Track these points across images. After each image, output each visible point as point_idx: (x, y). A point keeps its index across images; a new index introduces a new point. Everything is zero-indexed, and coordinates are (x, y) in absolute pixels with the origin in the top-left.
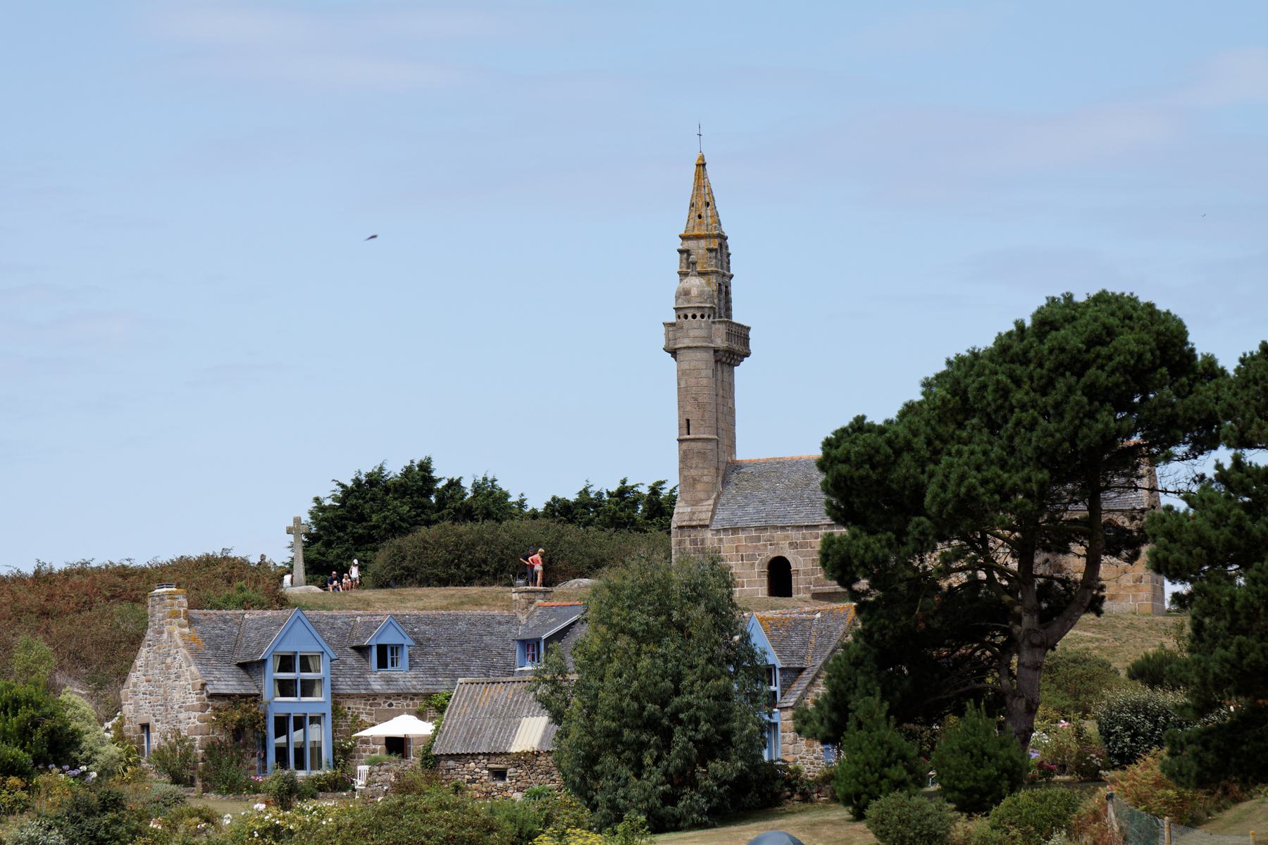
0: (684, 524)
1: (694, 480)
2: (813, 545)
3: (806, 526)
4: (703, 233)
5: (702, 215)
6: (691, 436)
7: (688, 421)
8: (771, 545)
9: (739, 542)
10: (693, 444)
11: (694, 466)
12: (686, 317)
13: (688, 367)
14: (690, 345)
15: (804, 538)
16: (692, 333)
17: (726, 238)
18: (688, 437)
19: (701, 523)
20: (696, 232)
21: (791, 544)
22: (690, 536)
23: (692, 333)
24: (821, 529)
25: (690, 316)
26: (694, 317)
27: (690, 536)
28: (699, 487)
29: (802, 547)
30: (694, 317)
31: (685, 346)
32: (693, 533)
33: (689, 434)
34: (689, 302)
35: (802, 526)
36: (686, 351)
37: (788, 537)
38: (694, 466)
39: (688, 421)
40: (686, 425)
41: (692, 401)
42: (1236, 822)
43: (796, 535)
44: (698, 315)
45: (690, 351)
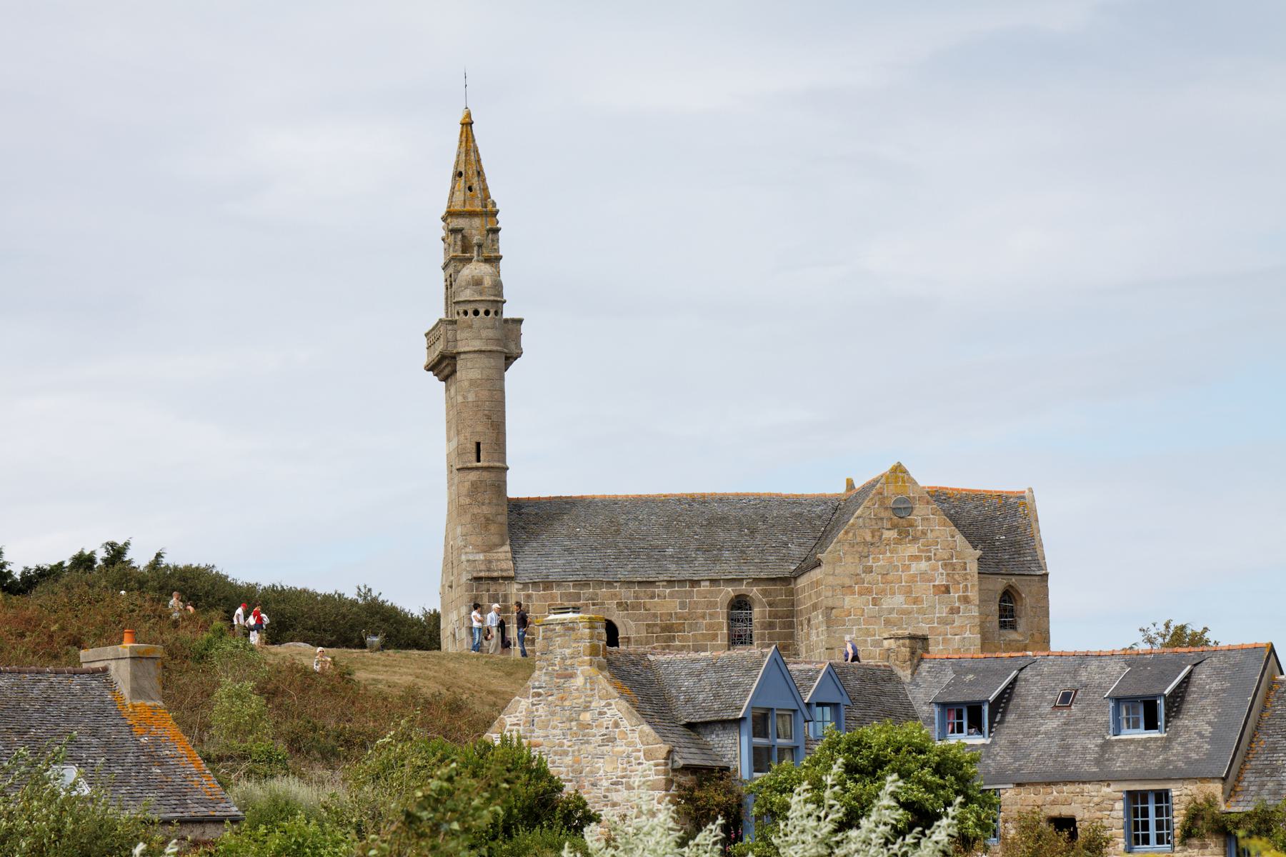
0: (482, 574)
2: (648, 607)
3: (639, 582)
7: (478, 444)
8: (594, 605)
9: (552, 599)
11: (487, 501)
12: (476, 313)
15: (637, 598)
19: (505, 574)
20: (468, 208)
21: (619, 604)
22: (488, 590)
24: (616, 587)
26: (487, 313)
27: (488, 590)
29: (633, 608)
31: (476, 349)
32: (493, 588)
33: (478, 460)
34: (481, 294)
35: (634, 582)
36: (476, 355)
37: (615, 595)
39: (478, 444)
40: (474, 450)
43: (627, 594)
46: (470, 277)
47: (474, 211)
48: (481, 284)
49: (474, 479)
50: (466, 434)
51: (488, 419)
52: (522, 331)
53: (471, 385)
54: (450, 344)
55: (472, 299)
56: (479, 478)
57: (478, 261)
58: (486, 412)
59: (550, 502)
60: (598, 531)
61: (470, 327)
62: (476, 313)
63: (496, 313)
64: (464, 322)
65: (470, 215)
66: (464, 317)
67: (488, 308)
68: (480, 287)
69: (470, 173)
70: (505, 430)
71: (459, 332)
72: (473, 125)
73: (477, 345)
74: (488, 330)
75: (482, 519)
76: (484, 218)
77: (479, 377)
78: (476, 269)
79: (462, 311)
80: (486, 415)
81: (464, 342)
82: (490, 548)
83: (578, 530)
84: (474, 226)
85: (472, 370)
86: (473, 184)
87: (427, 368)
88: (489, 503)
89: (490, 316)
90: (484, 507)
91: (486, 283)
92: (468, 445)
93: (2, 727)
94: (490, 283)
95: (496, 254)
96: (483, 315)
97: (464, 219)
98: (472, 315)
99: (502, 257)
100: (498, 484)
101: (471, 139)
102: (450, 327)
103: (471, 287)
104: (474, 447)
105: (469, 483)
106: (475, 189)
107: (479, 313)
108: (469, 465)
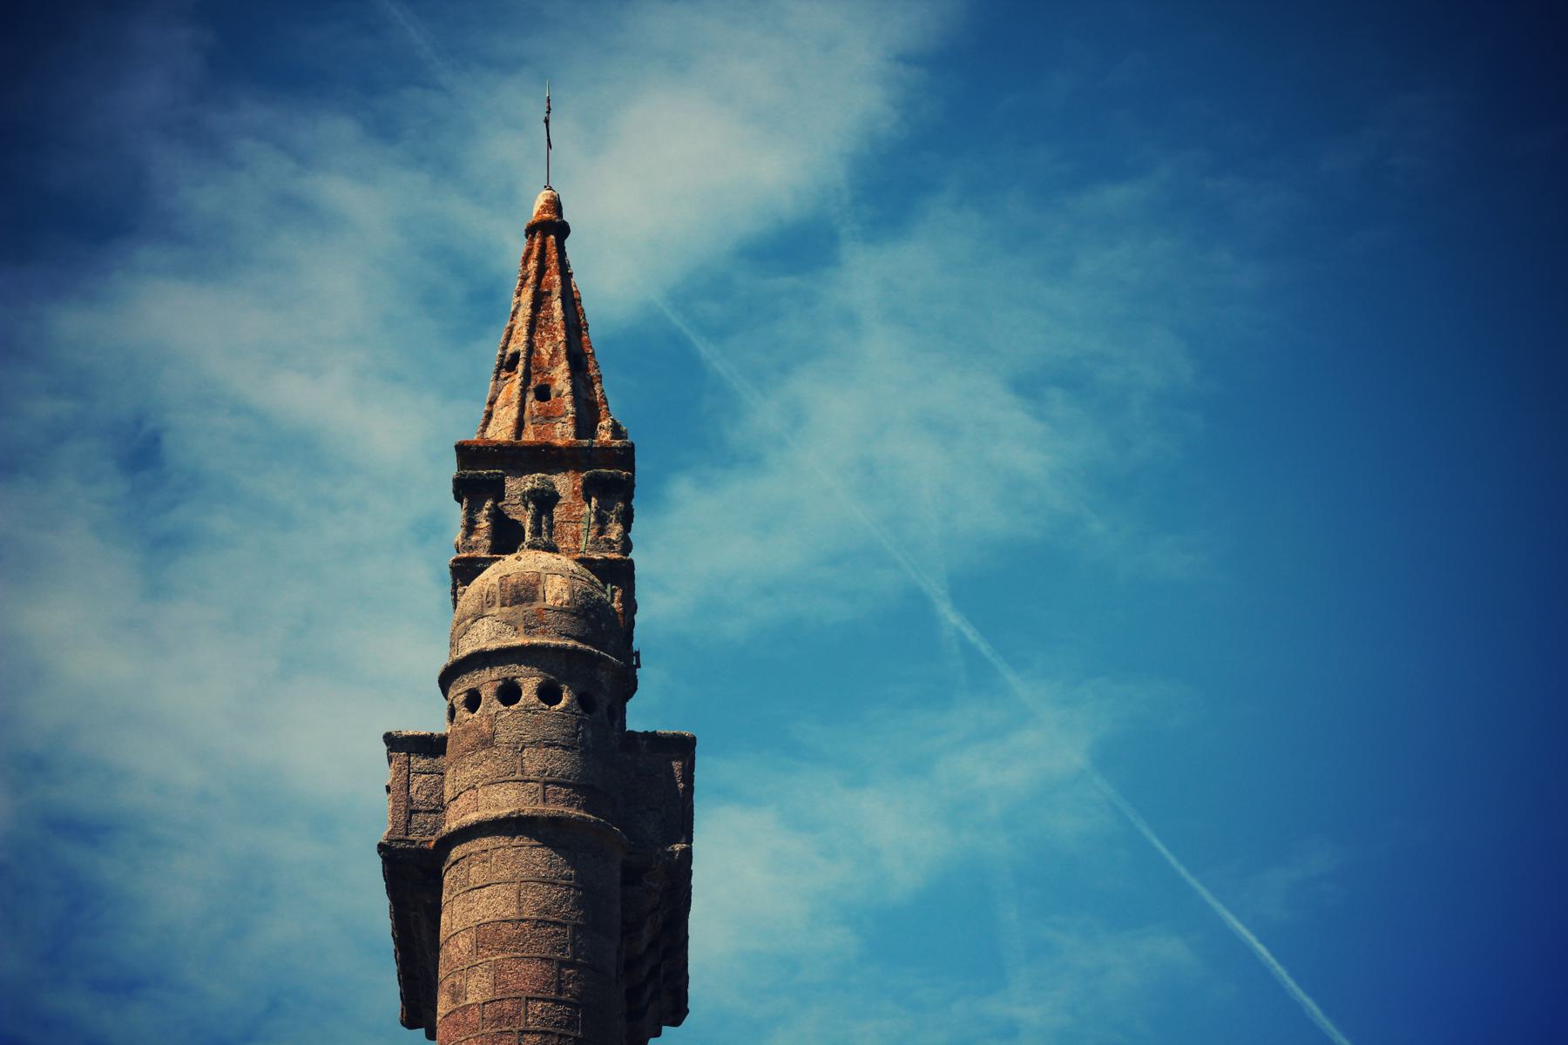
34: (529, 630)
48: (533, 599)
52: (642, 731)
53: (478, 945)
54: (418, 819)
61: (488, 742)
68: (525, 608)
69: (545, 352)
70: (688, 917)
71: (449, 774)
73: (505, 801)
77: (511, 912)
81: (461, 802)
82: (850, 320)
85: (486, 891)
86: (554, 380)
91: (549, 597)
98: (496, 703)
101: (553, 266)
102: (421, 763)
103: (496, 610)
106: (559, 395)
107: (520, 693)
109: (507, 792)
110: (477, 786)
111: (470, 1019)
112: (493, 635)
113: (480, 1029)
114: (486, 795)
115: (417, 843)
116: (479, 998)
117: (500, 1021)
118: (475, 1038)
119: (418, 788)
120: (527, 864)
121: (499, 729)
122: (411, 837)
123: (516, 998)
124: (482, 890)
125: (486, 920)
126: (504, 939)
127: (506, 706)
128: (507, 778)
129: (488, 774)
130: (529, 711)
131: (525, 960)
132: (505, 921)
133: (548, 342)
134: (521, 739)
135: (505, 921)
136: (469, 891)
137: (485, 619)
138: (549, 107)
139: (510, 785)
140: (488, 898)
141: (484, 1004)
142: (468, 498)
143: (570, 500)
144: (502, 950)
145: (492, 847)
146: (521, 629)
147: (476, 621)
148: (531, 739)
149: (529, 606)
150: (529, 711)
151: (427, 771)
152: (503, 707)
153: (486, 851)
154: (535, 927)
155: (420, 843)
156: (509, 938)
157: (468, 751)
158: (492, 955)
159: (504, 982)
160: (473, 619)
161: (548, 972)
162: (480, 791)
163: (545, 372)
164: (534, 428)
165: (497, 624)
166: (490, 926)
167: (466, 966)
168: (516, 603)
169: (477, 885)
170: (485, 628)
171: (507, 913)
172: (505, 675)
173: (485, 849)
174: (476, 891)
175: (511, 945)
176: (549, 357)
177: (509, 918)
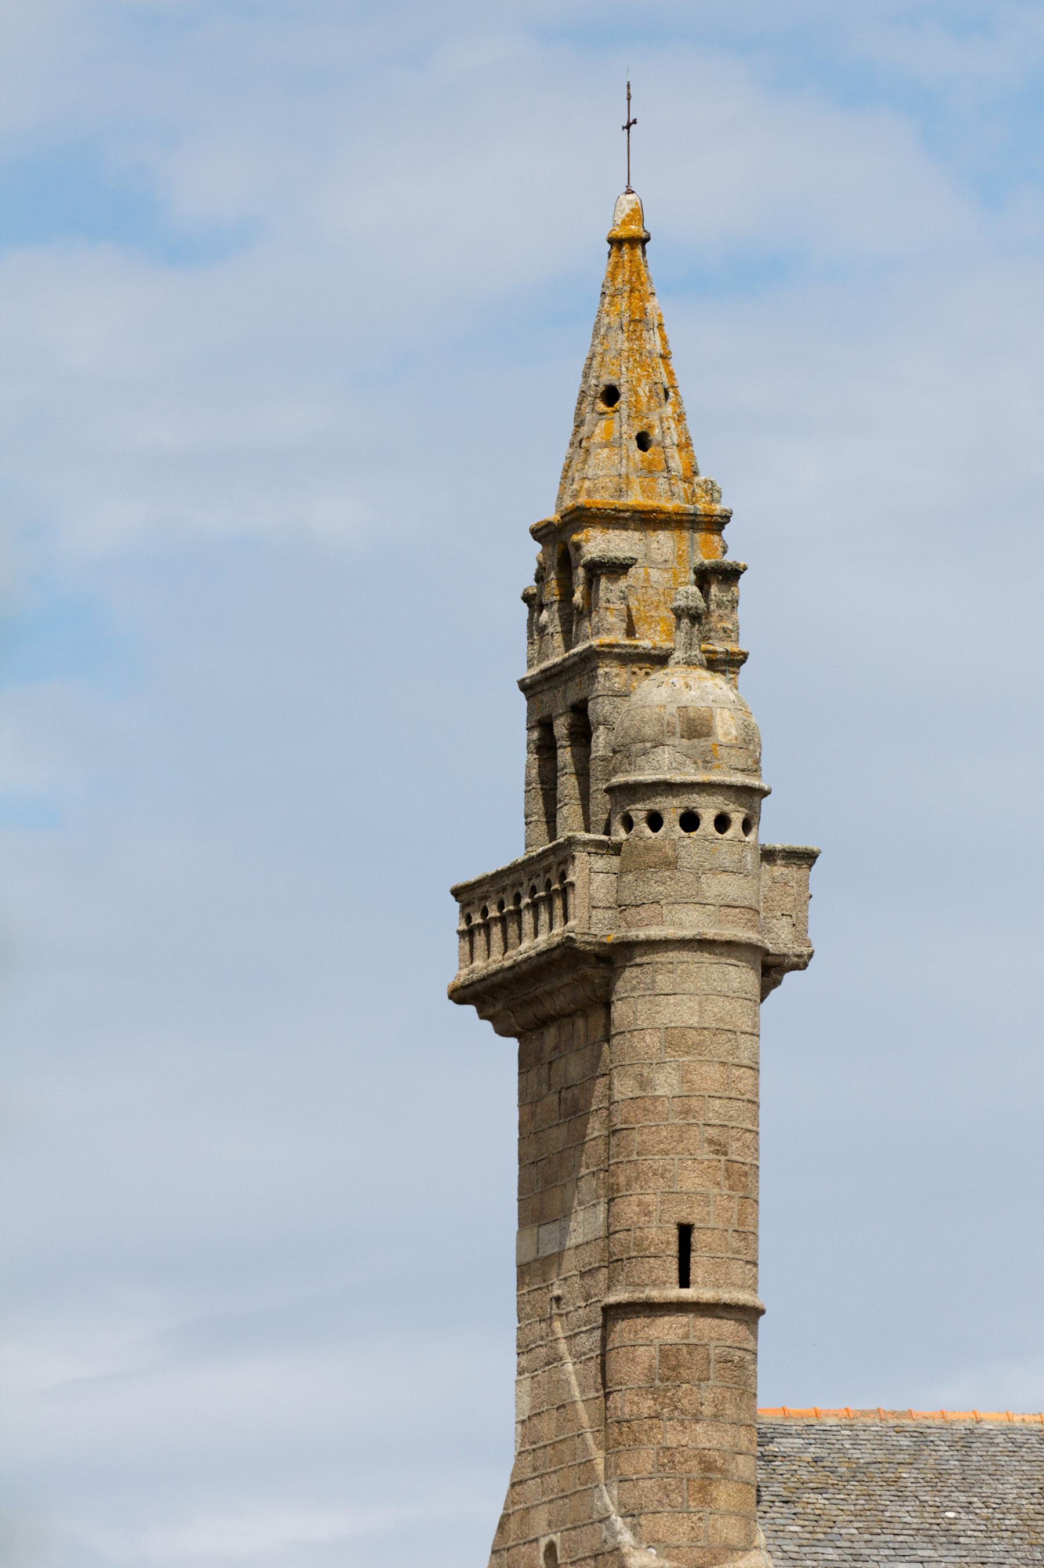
1: (708, 1466)
4: (670, 506)
5: (656, 434)
6: (688, 1294)
7: (685, 1231)
10: (705, 1325)
11: (707, 1410)
12: (690, 821)
13: (694, 1021)
14: (711, 933)
16: (716, 887)
17: (541, 533)
18: (675, 1293)
20: (635, 499)
23: (716, 887)
25: (707, 819)
26: (722, 823)
28: (724, 1494)
30: (722, 823)
31: (688, 933)
33: (684, 1281)
34: (707, 764)
36: (686, 956)
38: (707, 1410)
39: (685, 1231)
40: (674, 1249)
41: (705, 1153)
42: (782, 1559)
44: (737, 818)
45: (705, 957)
46: (672, 709)
47: (659, 511)
48: (708, 735)
49: (671, 1338)
50: (648, 1199)
51: (716, 1152)
55: (678, 778)
56: (687, 1336)
57: (689, 663)
58: (711, 1132)
59: (851, 1427)
60: (1011, 1521)
62: (690, 821)
63: (747, 826)
64: (648, 849)
65: (643, 520)
66: (648, 832)
67: (726, 809)
68: (702, 743)
72: (648, 245)
74: (724, 876)
75: (695, 1462)
76: (686, 534)
78: (687, 686)
79: (643, 814)
80: (711, 1141)
83: (951, 1515)
84: (656, 556)
87: (455, 995)
88: (715, 1416)
89: (730, 834)
90: (699, 1428)
92: (652, 1232)
93: (1040, 1523)
94: (734, 732)
95: (730, 647)
96: (712, 829)
97: (625, 534)
98: (678, 827)
99: (745, 656)
100: (742, 1360)
104: (674, 1233)
105: (654, 1351)
108: (655, 1294)
109: (690, 913)
110: (662, 902)
111: (660, 1108)
112: (674, 765)
113: (670, 1119)
114: (670, 913)
115: (598, 937)
116: (668, 1092)
117: (686, 1114)
118: (665, 1126)
119: (598, 887)
120: (707, 979)
121: (683, 854)
122: (592, 931)
123: (700, 1096)
124: (669, 997)
125: (673, 1025)
126: (690, 1043)
127: (686, 831)
128: (689, 900)
129: (672, 894)
130: (707, 840)
131: (708, 1063)
132: (690, 1028)
133: (644, 381)
134: (702, 866)
135: (690, 1028)
136: (656, 995)
137: (666, 748)
138: (629, 94)
139: (690, 906)
140: (675, 1006)
141: (673, 1097)
142: (571, 536)
143: (675, 564)
144: (688, 1053)
145: (677, 960)
146: (700, 764)
147: (655, 747)
148: (709, 867)
149: (706, 741)
150: (707, 840)
151: (604, 871)
152: (683, 833)
153: (672, 963)
154: (715, 1035)
155: (601, 937)
156: (693, 1043)
157: (651, 867)
158: (679, 1056)
159: (690, 1082)
160: (653, 744)
161: (724, 1074)
162: (664, 907)
163: (643, 417)
164: (640, 483)
165: (678, 754)
166: (677, 1031)
167: (655, 1062)
168: (694, 737)
169: (664, 993)
170: (666, 756)
171: (692, 1021)
172: (686, 804)
173: (671, 961)
174: (663, 996)
175: (695, 1049)
176: (646, 399)
177: (693, 1026)
